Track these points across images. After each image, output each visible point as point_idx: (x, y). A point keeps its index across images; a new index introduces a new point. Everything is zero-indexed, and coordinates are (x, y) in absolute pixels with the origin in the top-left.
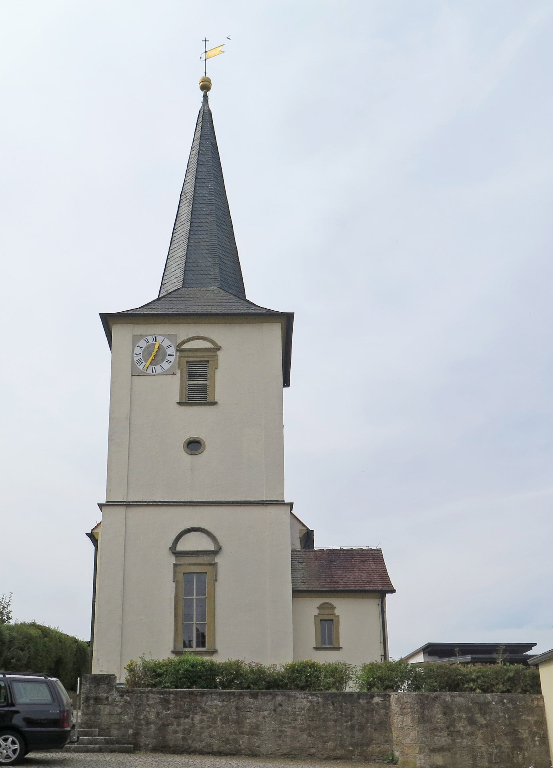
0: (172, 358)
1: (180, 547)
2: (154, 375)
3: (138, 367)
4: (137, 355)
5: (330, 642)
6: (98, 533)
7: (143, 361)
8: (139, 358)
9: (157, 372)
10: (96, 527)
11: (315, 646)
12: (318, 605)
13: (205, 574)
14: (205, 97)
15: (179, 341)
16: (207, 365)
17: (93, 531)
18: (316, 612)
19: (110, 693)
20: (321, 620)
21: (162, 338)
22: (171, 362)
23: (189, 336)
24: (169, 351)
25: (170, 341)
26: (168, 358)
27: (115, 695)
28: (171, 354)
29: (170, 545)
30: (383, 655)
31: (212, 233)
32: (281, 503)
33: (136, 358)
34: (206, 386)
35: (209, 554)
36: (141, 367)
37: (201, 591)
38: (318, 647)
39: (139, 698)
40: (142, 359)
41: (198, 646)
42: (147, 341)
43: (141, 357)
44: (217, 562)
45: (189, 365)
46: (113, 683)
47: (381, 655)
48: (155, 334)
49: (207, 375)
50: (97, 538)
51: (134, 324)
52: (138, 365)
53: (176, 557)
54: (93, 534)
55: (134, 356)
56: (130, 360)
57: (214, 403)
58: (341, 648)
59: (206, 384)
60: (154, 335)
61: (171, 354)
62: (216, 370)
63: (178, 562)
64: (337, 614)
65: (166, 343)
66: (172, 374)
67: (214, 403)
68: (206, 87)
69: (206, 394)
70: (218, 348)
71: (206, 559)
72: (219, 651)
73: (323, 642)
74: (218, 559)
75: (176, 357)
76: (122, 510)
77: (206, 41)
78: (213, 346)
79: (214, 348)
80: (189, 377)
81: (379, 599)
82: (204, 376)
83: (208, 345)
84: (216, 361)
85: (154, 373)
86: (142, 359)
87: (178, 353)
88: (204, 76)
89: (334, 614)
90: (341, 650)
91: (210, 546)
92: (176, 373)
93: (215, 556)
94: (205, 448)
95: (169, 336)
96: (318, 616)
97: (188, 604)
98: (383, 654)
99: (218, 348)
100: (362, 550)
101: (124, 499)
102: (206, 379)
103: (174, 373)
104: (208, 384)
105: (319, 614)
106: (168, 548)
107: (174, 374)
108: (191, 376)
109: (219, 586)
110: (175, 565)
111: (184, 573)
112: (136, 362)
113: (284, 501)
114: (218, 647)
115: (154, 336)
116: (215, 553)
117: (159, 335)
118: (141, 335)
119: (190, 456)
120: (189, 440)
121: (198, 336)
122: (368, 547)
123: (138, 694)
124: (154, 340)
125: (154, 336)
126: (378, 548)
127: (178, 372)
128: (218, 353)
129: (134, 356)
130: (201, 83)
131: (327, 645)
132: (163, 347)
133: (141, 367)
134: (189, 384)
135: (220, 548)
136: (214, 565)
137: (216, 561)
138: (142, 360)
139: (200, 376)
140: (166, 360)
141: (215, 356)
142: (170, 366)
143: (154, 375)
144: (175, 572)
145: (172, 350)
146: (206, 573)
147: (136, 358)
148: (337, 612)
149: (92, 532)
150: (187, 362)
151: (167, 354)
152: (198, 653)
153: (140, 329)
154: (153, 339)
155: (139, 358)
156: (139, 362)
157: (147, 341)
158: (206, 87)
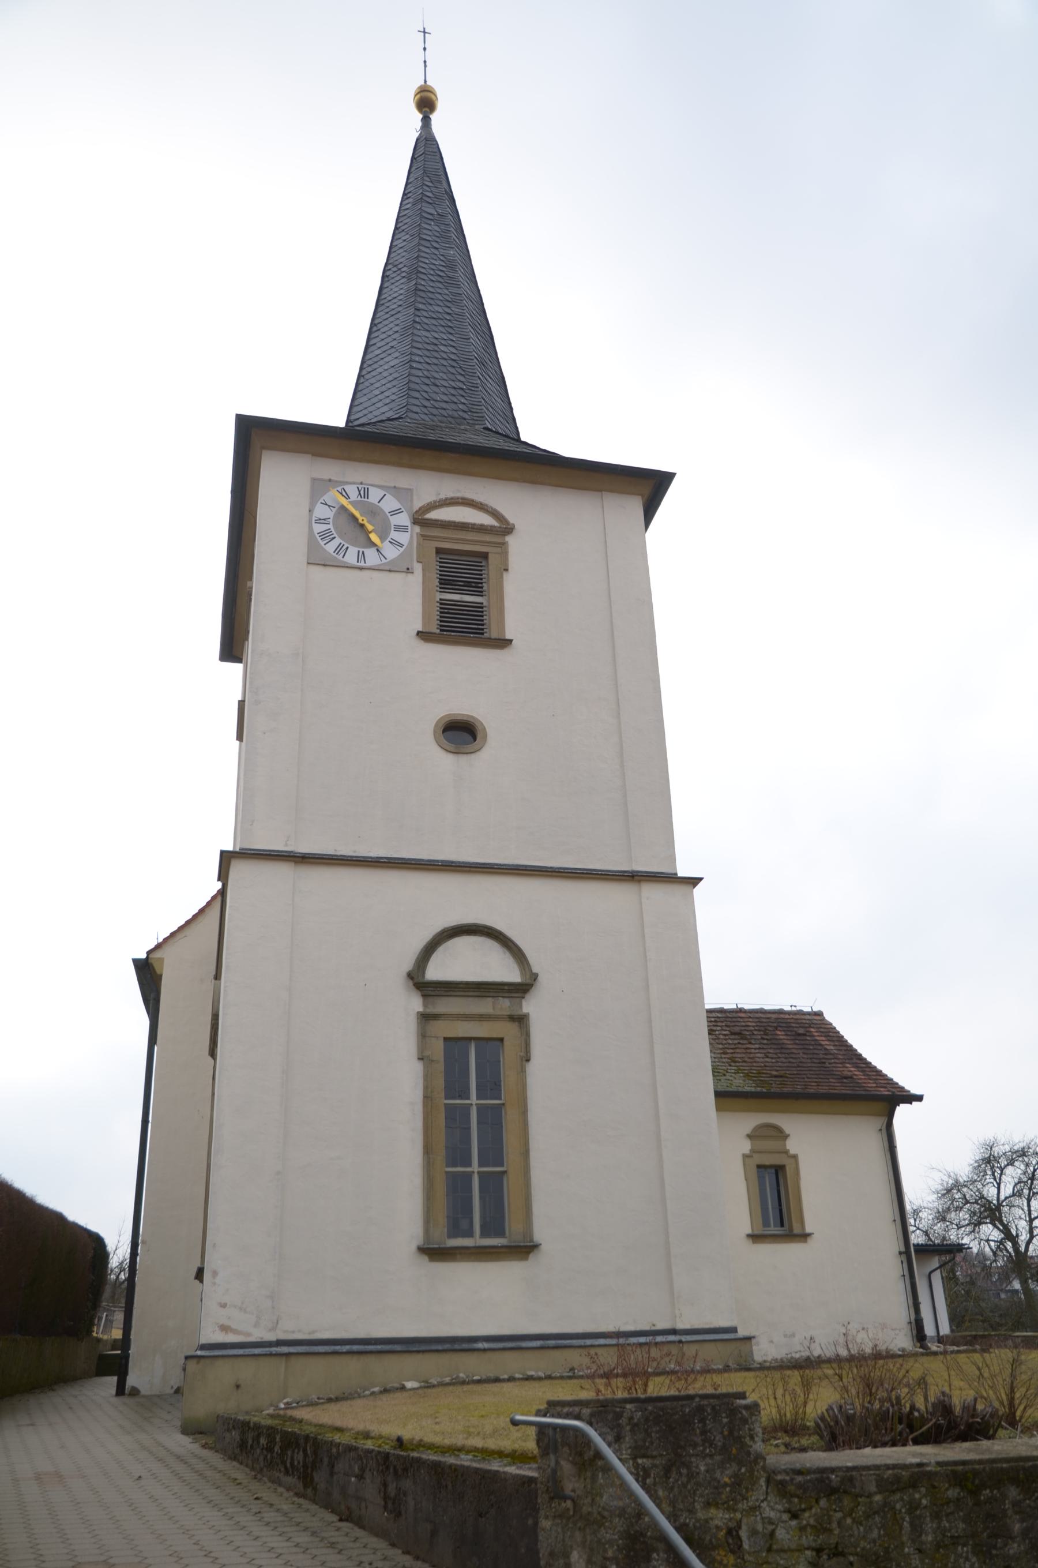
0: (404, 538)
1: (434, 972)
2: (361, 569)
3: (322, 547)
4: (319, 521)
5: (494, 1225)
6: (161, 960)
7: (335, 535)
8: (325, 527)
9: (369, 564)
10: (158, 946)
11: (749, 1231)
12: (748, 1130)
13: (498, 1043)
14: (426, 121)
15: (418, 504)
16: (481, 562)
17: (150, 956)
18: (746, 1147)
19: (743, 1506)
20: (759, 1167)
21: (382, 493)
22: (401, 545)
23: (442, 496)
24: (395, 520)
25: (399, 501)
26: (394, 535)
27: (769, 1513)
28: (400, 528)
29: (408, 963)
30: (904, 1253)
31: (462, 333)
32: (671, 878)
33: (318, 528)
34: (482, 608)
35: (509, 991)
36: (331, 548)
37: (490, 1085)
38: (756, 1232)
39: (877, 1519)
40: (332, 529)
41: (484, 1234)
42: (321, 521)
43: (331, 526)
44: (528, 1014)
45: (440, 558)
46: (747, 1440)
47: (900, 1253)
48: (364, 482)
49: (482, 583)
50: (158, 972)
51: (315, 454)
52: (322, 543)
53: (424, 996)
54: (150, 961)
55: (313, 521)
56: (306, 529)
57: (504, 643)
58: (809, 1235)
59: (482, 603)
60: (361, 483)
61: (400, 528)
62: (505, 574)
63: (431, 1010)
64: (792, 1152)
65: (390, 504)
66: (405, 570)
67: (504, 643)
68: (426, 103)
69: (483, 625)
70: (507, 529)
71: (504, 1005)
72: (544, 1247)
73: (458, 1225)
74: (530, 1006)
75: (412, 536)
76: (284, 871)
77: (424, 32)
78: (495, 523)
79: (500, 527)
80: (440, 584)
81: (883, 1118)
82: (476, 586)
83: (486, 520)
84: (504, 555)
85: (362, 564)
86: (332, 529)
87: (417, 529)
88: (423, 83)
89: (786, 1152)
90: (809, 1239)
91: (511, 974)
92: (412, 569)
93: (523, 998)
94: (486, 741)
95: (396, 491)
96: (752, 1156)
97: (456, 1118)
98: (903, 1249)
99: (507, 529)
100: (781, 1012)
101: (286, 845)
102: (482, 592)
103: (408, 569)
104: (484, 604)
105: (753, 1151)
106: (405, 974)
107: (409, 571)
108: (446, 584)
109: (536, 1070)
110: (425, 1018)
111: (445, 1039)
112: (317, 536)
113: (677, 874)
114: (541, 1232)
115: (360, 487)
116: (522, 989)
117: (372, 485)
118: (330, 480)
119: (451, 756)
120: (447, 720)
121: (463, 499)
122: (795, 1006)
123: (870, 1496)
124: (360, 494)
125: (360, 487)
126: (814, 1010)
127: (418, 568)
128: (510, 539)
129: (313, 521)
130: (418, 96)
131: (772, 1228)
132: (353, 545)
133: (331, 548)
134: (441, 600)
135: (535, 977)
136: (521, 1020)
137: (525, 1010)
138: (334, 532)
139: (468, 584)
140: (389, 539)
141: (503, 545)
142: (398, 553)
143: (361, 569)
144: (423, 1036)
145: (404, 519)
146: (501, 1040)
147: (318, 528)
148: (792, 1146)
149: (147, 957)
150: (439, 551)
151: (393, 527)
152: (488, 1250)
153: (329, 469)
154: (359, 491)
155: (325, 527)
156: (326, 536)
157: (321, 521)
158: (426, 103)
